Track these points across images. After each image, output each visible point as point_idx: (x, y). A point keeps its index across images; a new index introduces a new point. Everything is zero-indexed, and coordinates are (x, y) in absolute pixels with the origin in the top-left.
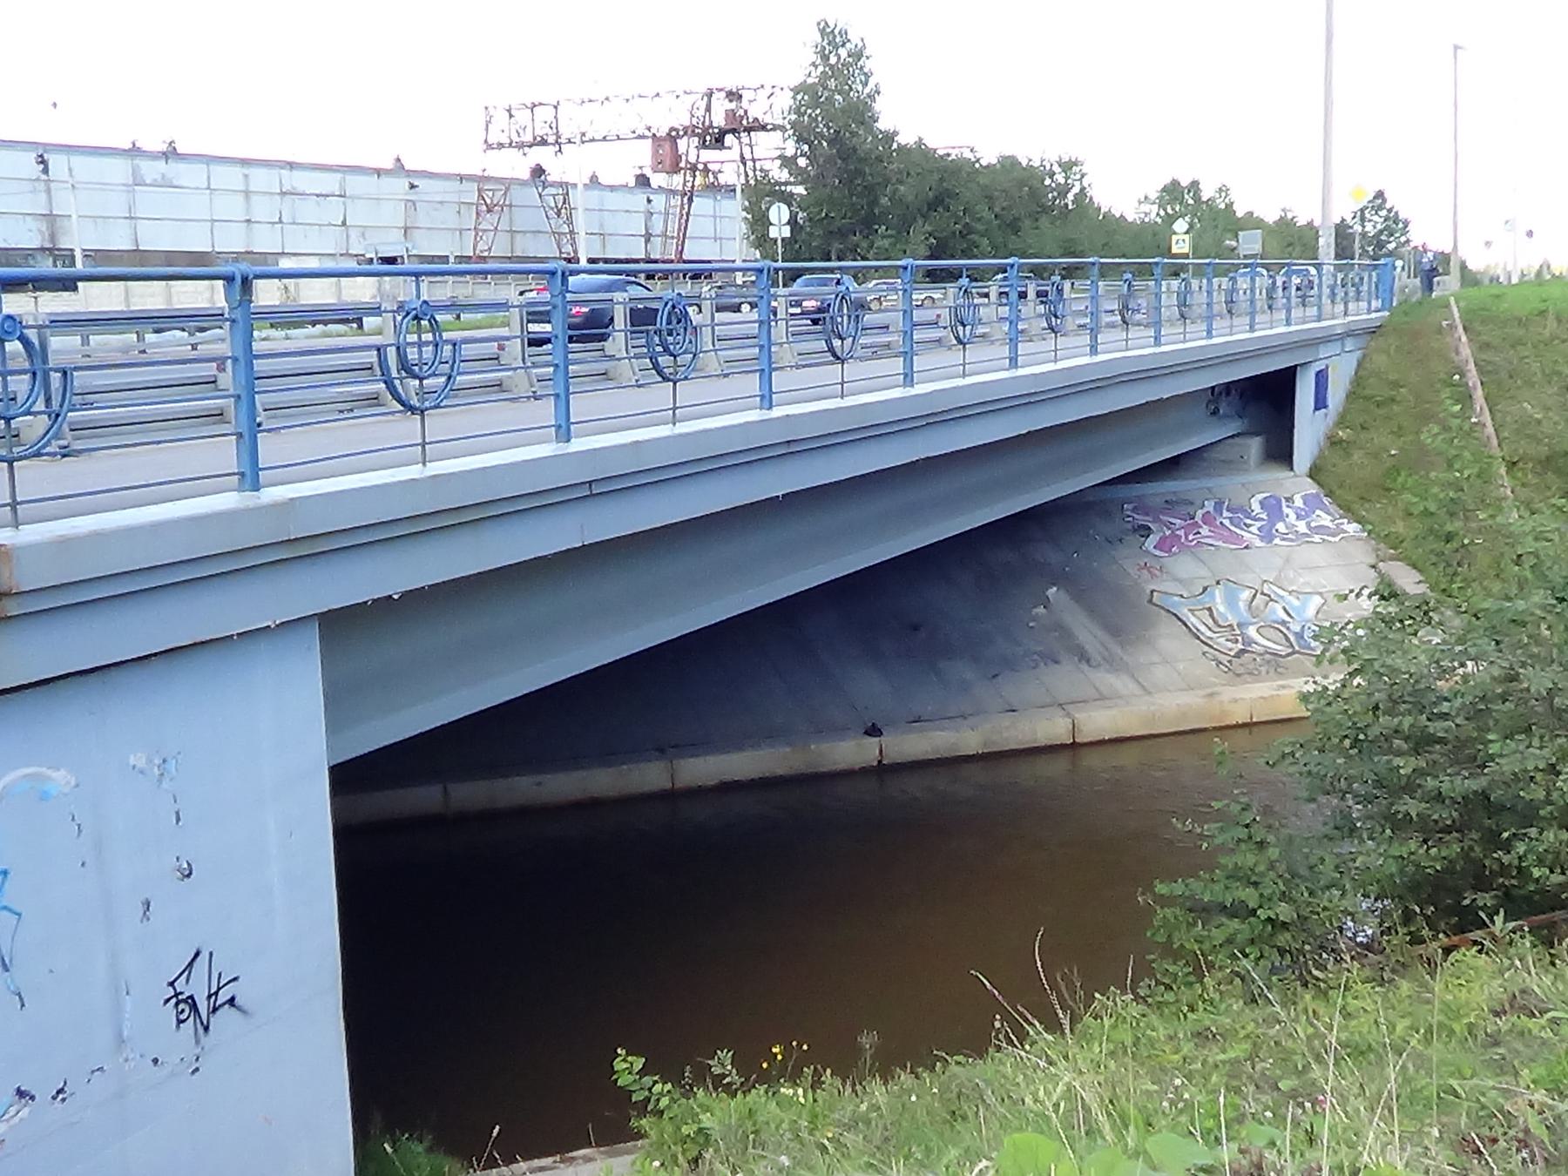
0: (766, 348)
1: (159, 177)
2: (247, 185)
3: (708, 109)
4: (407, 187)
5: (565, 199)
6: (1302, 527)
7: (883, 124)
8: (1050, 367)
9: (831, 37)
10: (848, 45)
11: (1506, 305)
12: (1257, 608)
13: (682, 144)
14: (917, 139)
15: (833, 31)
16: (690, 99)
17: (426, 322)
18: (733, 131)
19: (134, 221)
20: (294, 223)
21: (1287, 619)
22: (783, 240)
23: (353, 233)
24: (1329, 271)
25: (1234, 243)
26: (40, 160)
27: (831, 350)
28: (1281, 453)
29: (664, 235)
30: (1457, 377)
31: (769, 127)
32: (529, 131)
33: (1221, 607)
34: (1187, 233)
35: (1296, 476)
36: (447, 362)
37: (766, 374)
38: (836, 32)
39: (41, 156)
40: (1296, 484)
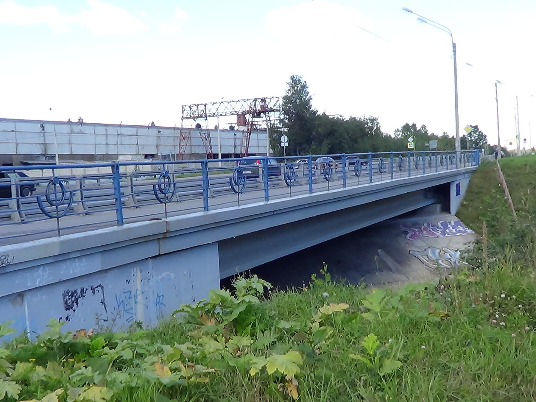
0: (345, 173)
1: (79, 131)
2: (106, 132)
3: (255, 105)
4: (157, 131)
5: (208, 135)
6: (454, 231)
7: (313, 108)
8: (288, 199)
9: (295, 81)
10: (301, 84)
11: (514, 163)
12: (442, 255)
13: (247, 116)
14: (323, 113)
15: (296, 79)
16: (249, 102)
17: (58, 185)
18: (263, 112)
19: (71, 145)
20: (121, 144)
21: (450, 258)
22: (286, 147)
23: (140, 147)
24: (459, 154)
25: (428, 144)
26: (42, 126)
27: (326, 178)
28: (446, 209)
29: (241, 145)
30: (500, 185)
31: (275, 110)
32: (197, 113)
33: (430, 254)
34: (413, 141)
35: (452, 216)
36: (68, 199)
37: (344, 180)
38: (297, 79)
39: (42, 125)
40: (452, 218)
